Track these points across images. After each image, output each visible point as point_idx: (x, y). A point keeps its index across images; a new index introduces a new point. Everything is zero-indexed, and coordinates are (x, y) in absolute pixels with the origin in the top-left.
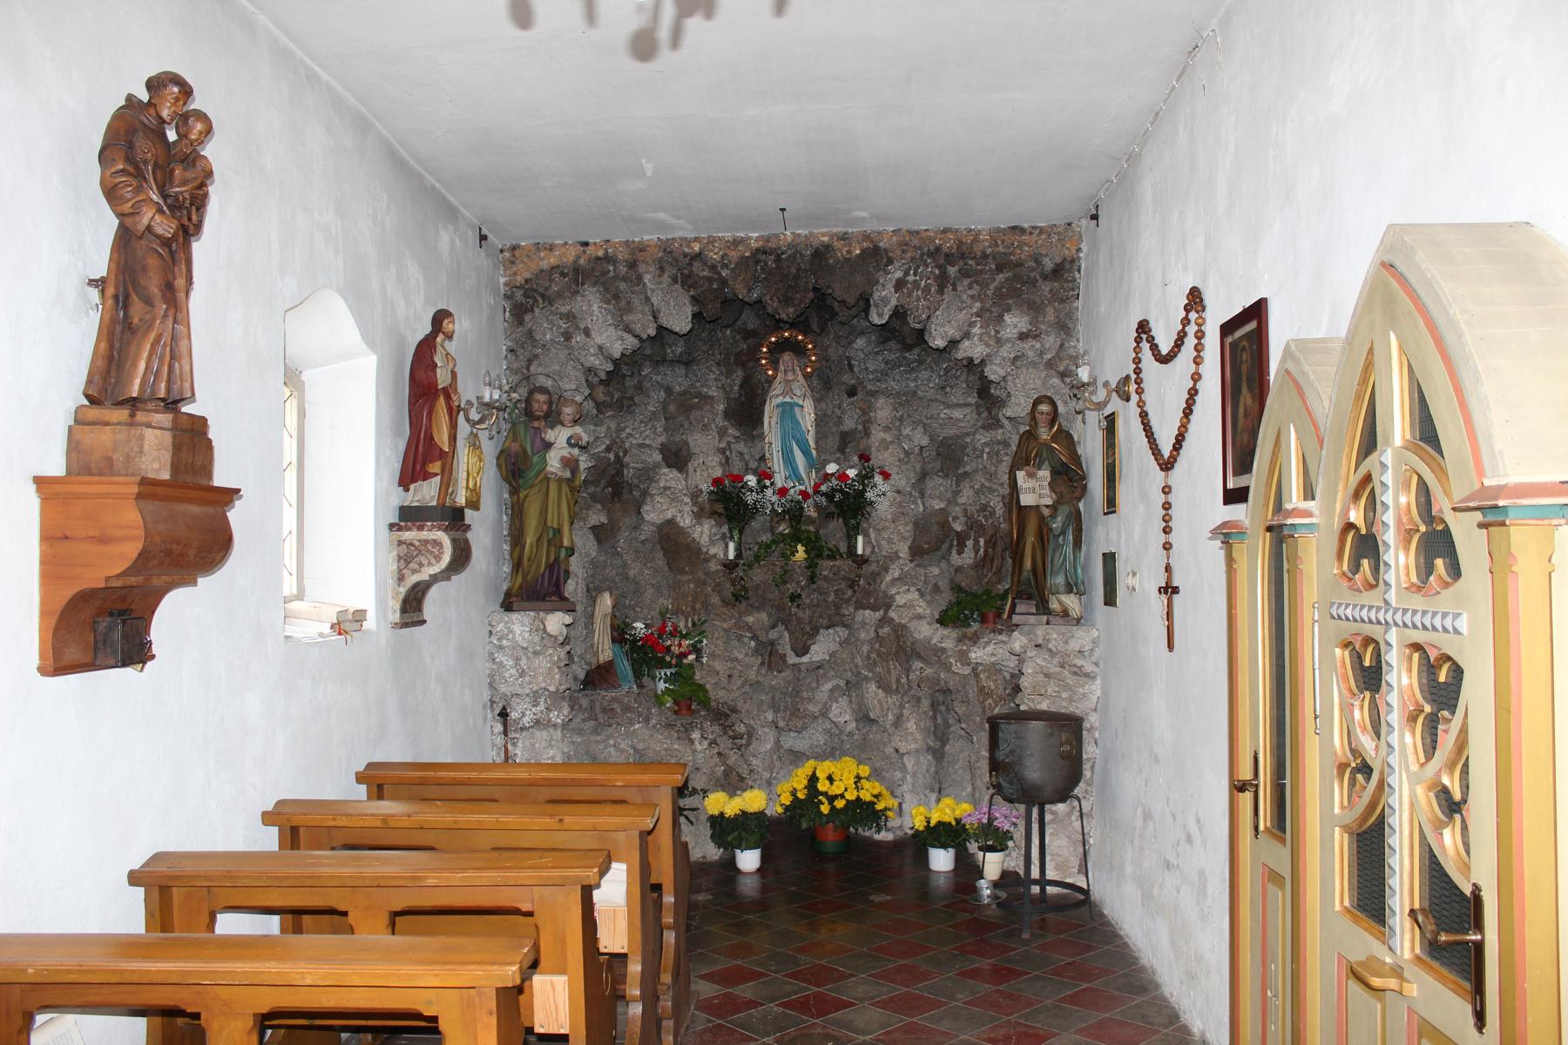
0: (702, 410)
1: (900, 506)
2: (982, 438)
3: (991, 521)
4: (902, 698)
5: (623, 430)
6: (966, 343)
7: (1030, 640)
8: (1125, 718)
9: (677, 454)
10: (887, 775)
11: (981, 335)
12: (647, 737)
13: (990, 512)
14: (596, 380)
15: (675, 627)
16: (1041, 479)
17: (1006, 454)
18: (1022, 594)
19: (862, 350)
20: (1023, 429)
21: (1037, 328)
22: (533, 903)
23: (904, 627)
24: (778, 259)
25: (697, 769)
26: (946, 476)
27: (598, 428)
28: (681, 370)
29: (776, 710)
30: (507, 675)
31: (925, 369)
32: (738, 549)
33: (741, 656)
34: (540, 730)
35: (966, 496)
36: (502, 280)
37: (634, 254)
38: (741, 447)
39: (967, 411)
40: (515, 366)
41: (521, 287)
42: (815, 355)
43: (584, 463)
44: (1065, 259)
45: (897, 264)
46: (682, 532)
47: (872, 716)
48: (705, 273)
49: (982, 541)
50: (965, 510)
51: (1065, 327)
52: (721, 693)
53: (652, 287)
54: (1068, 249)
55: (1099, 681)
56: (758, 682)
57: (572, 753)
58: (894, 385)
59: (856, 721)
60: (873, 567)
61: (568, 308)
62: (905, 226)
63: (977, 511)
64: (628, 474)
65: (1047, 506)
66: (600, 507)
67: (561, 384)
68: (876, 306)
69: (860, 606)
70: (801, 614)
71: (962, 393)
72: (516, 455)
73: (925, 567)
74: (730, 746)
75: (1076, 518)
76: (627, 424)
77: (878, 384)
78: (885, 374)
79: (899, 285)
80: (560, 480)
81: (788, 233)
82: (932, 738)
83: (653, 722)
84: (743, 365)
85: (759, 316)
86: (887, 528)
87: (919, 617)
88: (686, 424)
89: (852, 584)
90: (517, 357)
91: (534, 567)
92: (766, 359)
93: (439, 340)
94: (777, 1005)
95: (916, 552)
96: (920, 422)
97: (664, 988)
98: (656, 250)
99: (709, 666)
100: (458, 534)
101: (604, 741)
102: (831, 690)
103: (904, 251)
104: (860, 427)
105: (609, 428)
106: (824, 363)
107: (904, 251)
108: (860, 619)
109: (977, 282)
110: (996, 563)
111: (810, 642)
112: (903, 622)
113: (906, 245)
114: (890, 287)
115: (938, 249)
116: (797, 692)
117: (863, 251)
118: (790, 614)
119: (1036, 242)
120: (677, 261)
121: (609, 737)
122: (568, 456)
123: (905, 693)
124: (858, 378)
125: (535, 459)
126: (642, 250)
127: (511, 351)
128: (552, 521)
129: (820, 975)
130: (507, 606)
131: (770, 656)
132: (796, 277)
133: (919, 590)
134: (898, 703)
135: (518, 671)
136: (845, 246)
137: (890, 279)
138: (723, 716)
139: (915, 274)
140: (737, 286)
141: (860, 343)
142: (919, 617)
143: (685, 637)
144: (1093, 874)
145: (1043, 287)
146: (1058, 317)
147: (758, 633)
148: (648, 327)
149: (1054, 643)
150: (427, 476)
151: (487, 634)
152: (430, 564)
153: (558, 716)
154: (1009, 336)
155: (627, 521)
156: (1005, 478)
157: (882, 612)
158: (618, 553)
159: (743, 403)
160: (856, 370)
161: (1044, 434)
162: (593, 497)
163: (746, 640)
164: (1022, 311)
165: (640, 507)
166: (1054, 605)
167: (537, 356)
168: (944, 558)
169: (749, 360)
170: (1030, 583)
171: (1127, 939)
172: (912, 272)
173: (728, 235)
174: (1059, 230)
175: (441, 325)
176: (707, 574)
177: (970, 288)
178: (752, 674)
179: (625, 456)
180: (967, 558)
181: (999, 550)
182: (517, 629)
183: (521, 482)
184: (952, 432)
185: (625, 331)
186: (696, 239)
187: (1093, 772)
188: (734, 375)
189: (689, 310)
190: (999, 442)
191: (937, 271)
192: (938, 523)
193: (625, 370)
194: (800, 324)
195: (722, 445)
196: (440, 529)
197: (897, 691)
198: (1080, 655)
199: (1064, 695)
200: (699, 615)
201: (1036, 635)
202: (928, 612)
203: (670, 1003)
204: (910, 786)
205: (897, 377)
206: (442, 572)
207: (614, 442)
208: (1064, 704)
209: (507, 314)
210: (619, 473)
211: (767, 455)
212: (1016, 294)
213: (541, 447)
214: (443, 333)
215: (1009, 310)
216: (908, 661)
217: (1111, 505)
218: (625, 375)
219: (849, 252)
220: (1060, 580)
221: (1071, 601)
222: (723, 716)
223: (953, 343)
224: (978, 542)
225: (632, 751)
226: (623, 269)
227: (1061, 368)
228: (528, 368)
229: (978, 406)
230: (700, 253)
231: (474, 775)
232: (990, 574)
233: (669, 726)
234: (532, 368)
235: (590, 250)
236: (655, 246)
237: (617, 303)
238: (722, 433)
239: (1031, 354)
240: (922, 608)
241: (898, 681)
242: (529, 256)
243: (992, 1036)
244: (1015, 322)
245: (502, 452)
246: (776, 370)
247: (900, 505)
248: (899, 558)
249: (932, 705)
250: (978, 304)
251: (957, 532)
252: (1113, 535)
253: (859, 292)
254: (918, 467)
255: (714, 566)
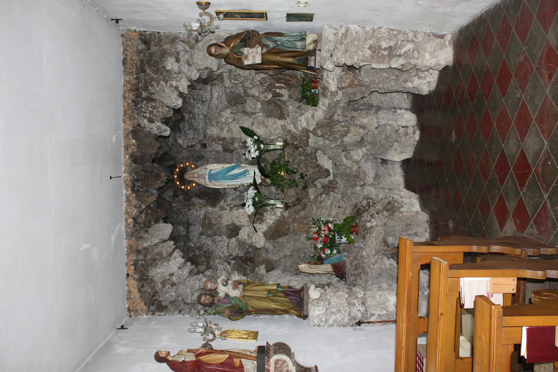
0: (211, 218)
1: (259, 124)
2: (227, 83)
3: (267, 80)
4: (351, 125)
5: (220, 256)
6: (180, 89)
7: (328, 60)
8: (371, 10)
9: (232, 231)
10: (388, 133)
11: (176, 81)
12: (370, 249)
13: (264, 80)
14: (196, 270)
15: (315, 233)
16: (248, 53)
17: (236, 71)
18: (305, 64)
19: (184, 140)
20: (223, 62)
21: (174, 53)
22: (509, 345)
23: (317, 123)
24: (137, 180)
25: (385, 224)
26: (245, 101)
27: (219, 269)
28: (192, 228)
29: (355, 185)
30: (340, 319)
31: (194, 110)
32: (412, 274)
33: (330, 202)
34: (367, 302)
35: (255, 92)
36: (145, 316)
37: (133, 251)
38: (229, 199)
39: (214, 90)
40: (188, 310)
41: (149, 307)
42: (186, 163)
43: (236, 277)
44: (140, 38)
45: (141, 122)
46: (270, 228)
47: (359, 140)
48: (143, 216)
49: (277, 85)
50: (262, 92)
51: (174, 40)
52: (347, 211)
53: (149, 243)
54: (134, 36)
55: (350, 26)
56: (342, 194)
57: (377, 286)
58: (201, 125)
59: (362, 147)
60: (289, 137)
61: (159, 284)
62: (121, 117)
63: (263, 87)
64: (241, 254)
65: (262, 50)
66: (257, 268)
67: (196, 288)
68: (161, 132)
69: (307, 144)
70: (310, 173)
71: (205, 92)
72: (232, 312)
73: (289, 113)
74: (373, 208)
75: (268, 35)
76: (217, 254)
77: (200, 133)
78: (195, 130)
79: (151, 121)
80: (244, 290)
81: (124, 175)
82: (370, 111)
83: (362, 245)
84: (191, 197)
85: (167, 190)
86: (270, 130)
87: (313, 116)
88: (218, 226)
89: (297, 147)
90: (183, 309)
91: (286, 304)
92: (187, 187)
93: (170, 359)
94: (522, 191)
95: (282, 117)
96: (219, 114)
97: (523, 253)
98: (132, 241)
99: (334, 217)
100: (272, 350)
101: (371, 269)
102: (347, 159)
103: (134, 118)
104: (221, 142)
105: (219, 263)
106: (190, 159)
107: (134, 118)
108: (313, 144)
109: (150, 83)
110: (288, 78)
111: (324, 169)
112: (315, 124)
113: (131, 117)
114: (152, 125)
115: (133, 101)
116: (347, 175)
117: (134, 138)
118: (310, 178)
119: (131, 52)
120: (137, 230)
121: (369, 267)
122: (232, 286)
123: (349, 123)
124: (198, 143)
125: (233, 302)
126: (131, 248)
127: (180, 312)
128: (264, 294)
129: (503, 167)
130: (305, 317)
131: (330, 188)
132: (146, 171)
133: (300, 116)
134: (354, 127)
135: (338, 313)
136: (131, 147)
137: (148, 125)
138: (359, 212)
139: (146, 113)
140: (150, 201)
141: (180, 141)
142: (313, 116)
143: (320, 229)
144: (445, 31)
145: (153, 50)
146: (168, 43)
147: (318, 193)
148: (169, 245)
149: (330, 47)
150: (241, 366)
151: (319, 328)
152: (287, 366)
153: (360, 293)
154: (177, 67)
155: (264, 255)
156: (247, 72)
157: (310, 134)
158: (280, 259)
159: (208, 198)
160: (193, 143)
161: (226, 51)
162: (253, 271)
163: (322, 199)
164: (165, 61)
165: (257, 248)
166: (311, 47)
167: (183, 300)
168: (284, 104)
169: (188, 194)
170: (300, 59)
171: (483, 12)
172: (145, 114)
173: (124, 205)
174: (125, 40)
175: (163, 358)
176: (290, 217)
177: (153, 86)
178: (339, 196)
179: (232, 256)
180: (285, 92)
181: (281, 77)
182: (317, 313)
183: (244, 309)
184: (224, 98)
185: (171, 256)
186: (126, 221)
187: (394, 30)
188: (195, 202)
189: (161, 225)
190: (230, 75)
191: (145, 102)
192: (268, 105)
193: (191, 255)
194: (172, 169)
195: (228, 209)
196: (269, 361)
197: (348, 127)
198: (337, 35)
199: (356, 43)
200: (309, 221)
201: (326, 57)
202: (311, 111)
203: (532, 250)
204: (394, 122)
205: (197, 123)
206: (291, 359)
207: (226, 261)
208: (360, 43)
209: (162, 314)
210: (241, 258)
211: (233, 187)
212: (157, 63)
213: (228, 299)
214: (167, 356)
215: (164, 67)
216: (334, 122)
217: (262, 16)
218: (194, 254)
219: (134, 145)
220: (299, 44)
221: (310, 38)
222: (359, 212)
223: (181, 95)
224: (278, 87)
225: (376, 256)
226: (141, 257)
227: (194, 42)
228: (188, 304)
229: (212, 85)
230: (133, 219)
231: (403, 352)
232: (293, 81)
233: (364, 237)
234: (189, 302)
235: (131, 273)
236: (129, 240)
237: (157, 260)
238: (223, 208)
239: (186, 57)
240: (309, 114)
241: (344, 127)
242: (133, 303)
243: (547, 76)
244: (170, 64)
245: (229, 318)
246: (193, 182)
247: (259, 124)
248: (284, 125)
249: (355, 110)
250: (161, 82)
251: (272, 97)
252: (277, 15)
253: (154, 141)
254: (240, 115)
255: (286, 214)
